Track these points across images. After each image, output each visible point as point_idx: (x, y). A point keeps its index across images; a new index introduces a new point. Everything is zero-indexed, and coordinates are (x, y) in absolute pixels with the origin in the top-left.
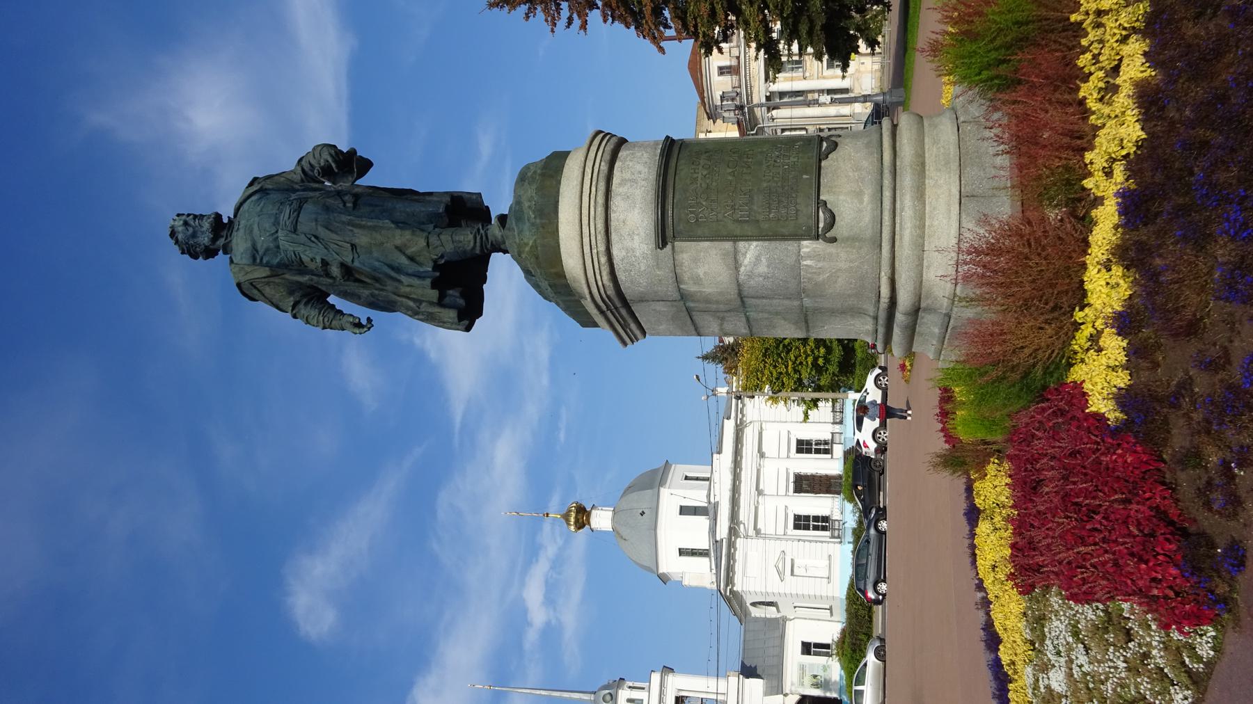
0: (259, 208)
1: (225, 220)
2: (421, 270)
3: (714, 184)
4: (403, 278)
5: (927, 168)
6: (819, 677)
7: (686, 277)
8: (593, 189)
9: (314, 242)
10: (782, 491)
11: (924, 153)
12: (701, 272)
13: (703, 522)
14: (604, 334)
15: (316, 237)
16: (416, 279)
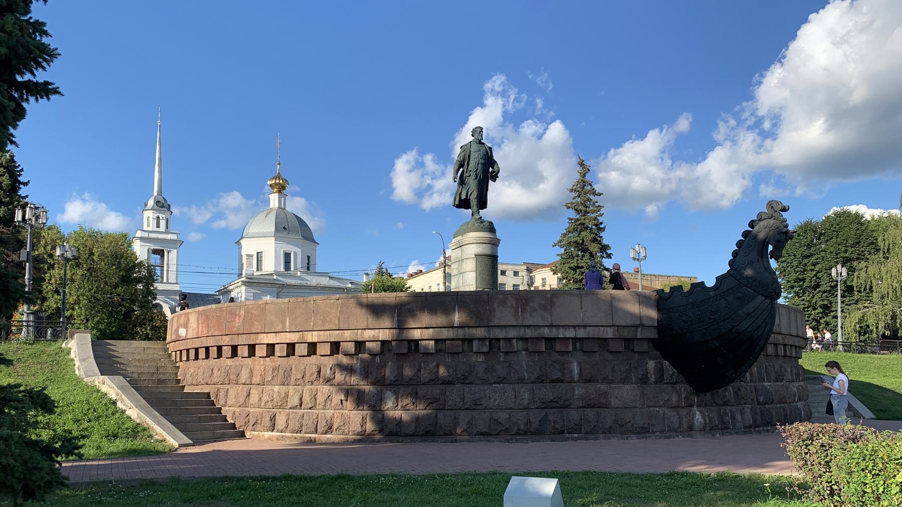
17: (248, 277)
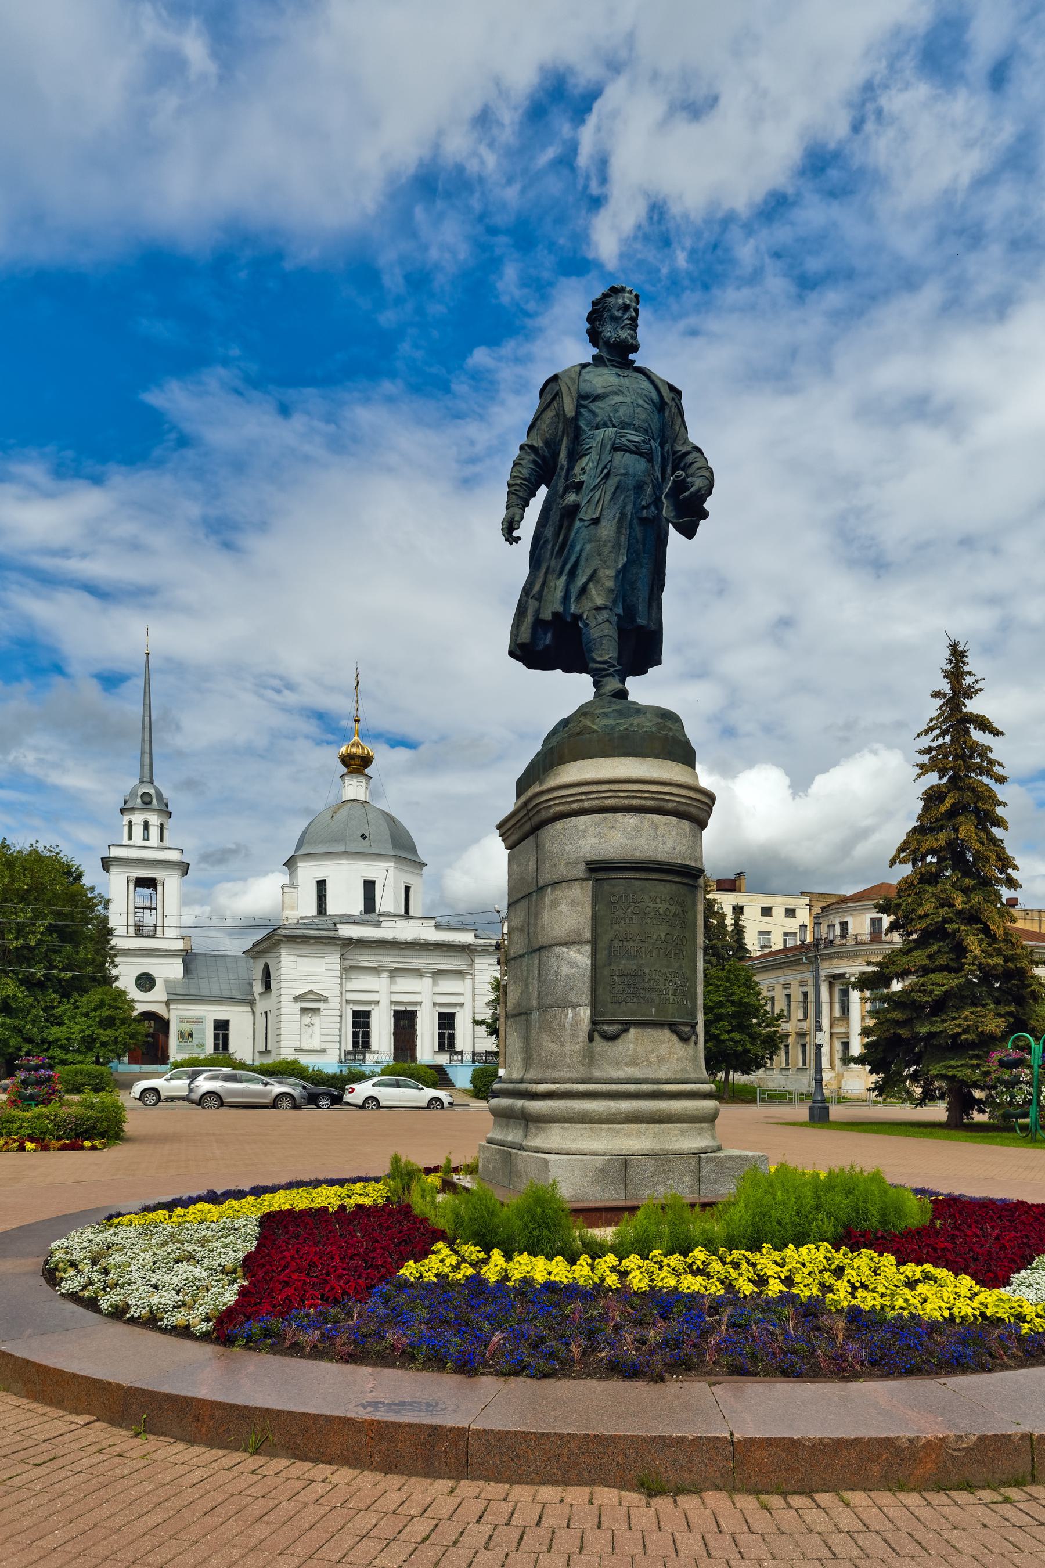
0: (641, 402)
1: (631, 356)
2: (572, 600)
3: (649, 921)
4: (564, 578)
5: (657, 1125)
6: (190, 1039)
7: (558, 892)
8: (647, 795)
9: (602, 472)
10: (397, 998)
11: (672, 1123)
12: (563, 908)
13: (357, 907)
14: (507, 803)
15: (607, 476)
16: (562, 594)
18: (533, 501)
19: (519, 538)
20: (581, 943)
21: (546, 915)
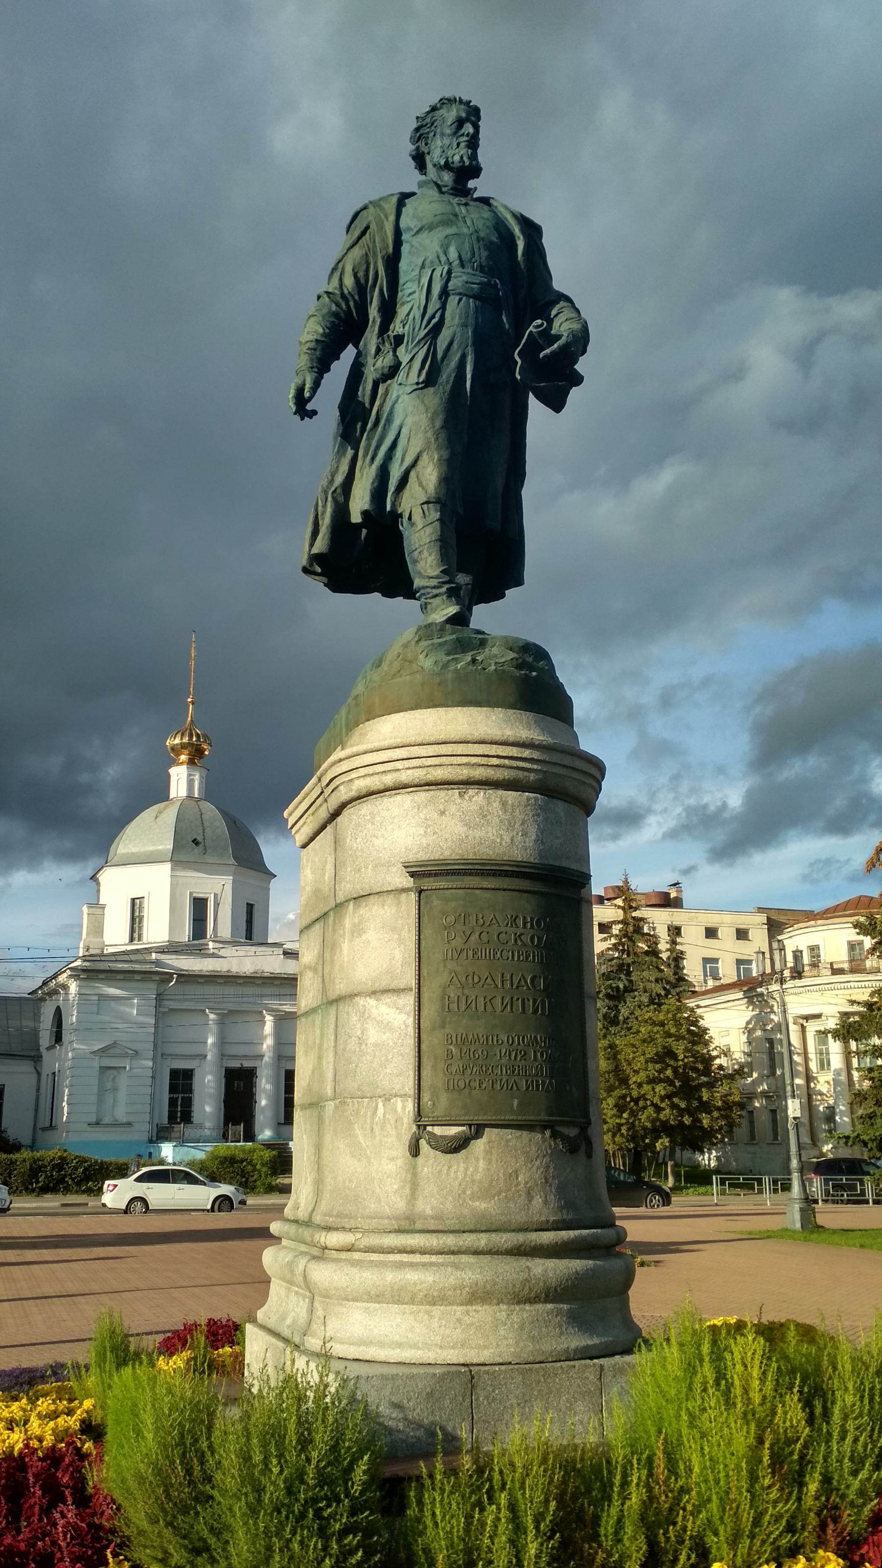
1: (471, 184)
7: (362, 911)
17: (87, 958)
18: (335, 365)
19: (314, 413)
20: (398, 991)
21: (345, 947)
